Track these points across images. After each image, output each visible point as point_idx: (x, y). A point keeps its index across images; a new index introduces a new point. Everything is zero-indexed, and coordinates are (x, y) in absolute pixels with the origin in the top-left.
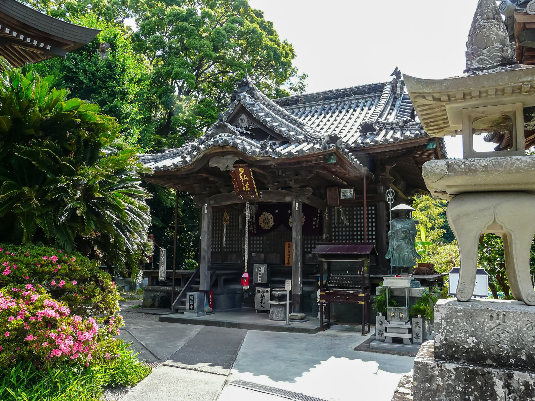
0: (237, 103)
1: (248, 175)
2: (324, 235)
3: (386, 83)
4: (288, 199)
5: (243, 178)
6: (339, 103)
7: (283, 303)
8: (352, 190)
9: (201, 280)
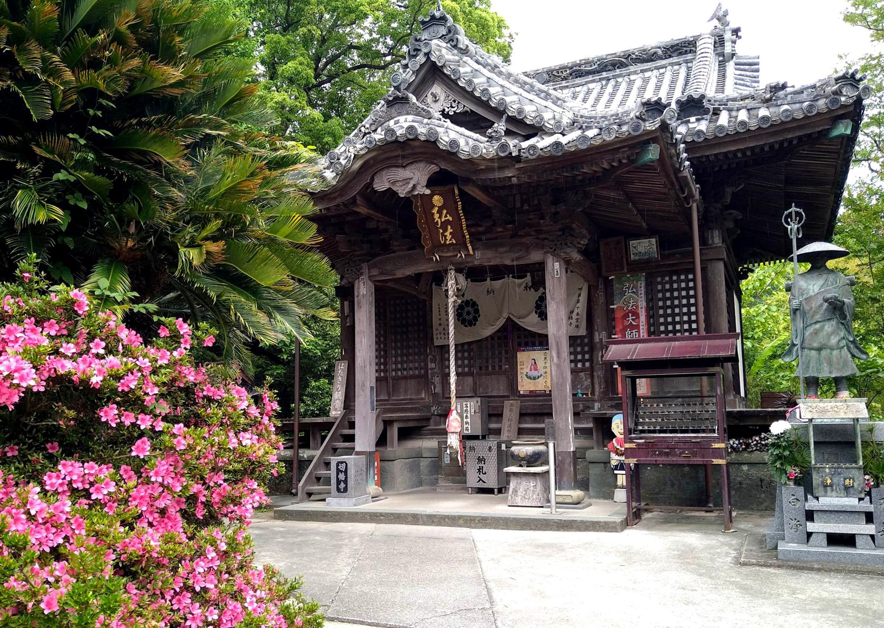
0: (424, 60)
1: (453, 211)
2: (597, 334)
3: (700, 36)
4: (535, 257)
5: (440, 217)
6: (604, 82)
7: (544, 468)
8: (653, 240)
9: (358, 432)
